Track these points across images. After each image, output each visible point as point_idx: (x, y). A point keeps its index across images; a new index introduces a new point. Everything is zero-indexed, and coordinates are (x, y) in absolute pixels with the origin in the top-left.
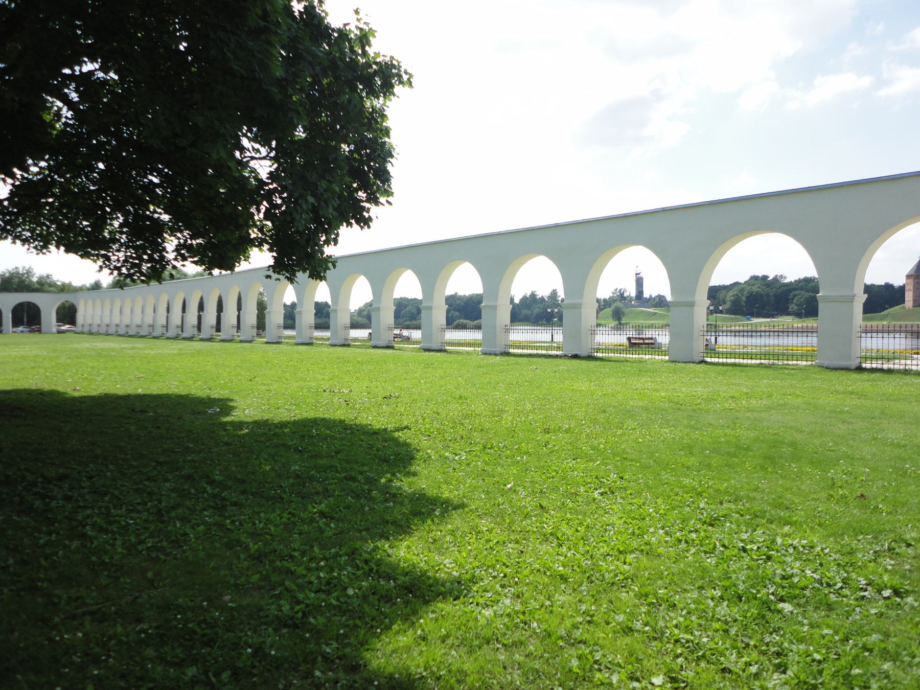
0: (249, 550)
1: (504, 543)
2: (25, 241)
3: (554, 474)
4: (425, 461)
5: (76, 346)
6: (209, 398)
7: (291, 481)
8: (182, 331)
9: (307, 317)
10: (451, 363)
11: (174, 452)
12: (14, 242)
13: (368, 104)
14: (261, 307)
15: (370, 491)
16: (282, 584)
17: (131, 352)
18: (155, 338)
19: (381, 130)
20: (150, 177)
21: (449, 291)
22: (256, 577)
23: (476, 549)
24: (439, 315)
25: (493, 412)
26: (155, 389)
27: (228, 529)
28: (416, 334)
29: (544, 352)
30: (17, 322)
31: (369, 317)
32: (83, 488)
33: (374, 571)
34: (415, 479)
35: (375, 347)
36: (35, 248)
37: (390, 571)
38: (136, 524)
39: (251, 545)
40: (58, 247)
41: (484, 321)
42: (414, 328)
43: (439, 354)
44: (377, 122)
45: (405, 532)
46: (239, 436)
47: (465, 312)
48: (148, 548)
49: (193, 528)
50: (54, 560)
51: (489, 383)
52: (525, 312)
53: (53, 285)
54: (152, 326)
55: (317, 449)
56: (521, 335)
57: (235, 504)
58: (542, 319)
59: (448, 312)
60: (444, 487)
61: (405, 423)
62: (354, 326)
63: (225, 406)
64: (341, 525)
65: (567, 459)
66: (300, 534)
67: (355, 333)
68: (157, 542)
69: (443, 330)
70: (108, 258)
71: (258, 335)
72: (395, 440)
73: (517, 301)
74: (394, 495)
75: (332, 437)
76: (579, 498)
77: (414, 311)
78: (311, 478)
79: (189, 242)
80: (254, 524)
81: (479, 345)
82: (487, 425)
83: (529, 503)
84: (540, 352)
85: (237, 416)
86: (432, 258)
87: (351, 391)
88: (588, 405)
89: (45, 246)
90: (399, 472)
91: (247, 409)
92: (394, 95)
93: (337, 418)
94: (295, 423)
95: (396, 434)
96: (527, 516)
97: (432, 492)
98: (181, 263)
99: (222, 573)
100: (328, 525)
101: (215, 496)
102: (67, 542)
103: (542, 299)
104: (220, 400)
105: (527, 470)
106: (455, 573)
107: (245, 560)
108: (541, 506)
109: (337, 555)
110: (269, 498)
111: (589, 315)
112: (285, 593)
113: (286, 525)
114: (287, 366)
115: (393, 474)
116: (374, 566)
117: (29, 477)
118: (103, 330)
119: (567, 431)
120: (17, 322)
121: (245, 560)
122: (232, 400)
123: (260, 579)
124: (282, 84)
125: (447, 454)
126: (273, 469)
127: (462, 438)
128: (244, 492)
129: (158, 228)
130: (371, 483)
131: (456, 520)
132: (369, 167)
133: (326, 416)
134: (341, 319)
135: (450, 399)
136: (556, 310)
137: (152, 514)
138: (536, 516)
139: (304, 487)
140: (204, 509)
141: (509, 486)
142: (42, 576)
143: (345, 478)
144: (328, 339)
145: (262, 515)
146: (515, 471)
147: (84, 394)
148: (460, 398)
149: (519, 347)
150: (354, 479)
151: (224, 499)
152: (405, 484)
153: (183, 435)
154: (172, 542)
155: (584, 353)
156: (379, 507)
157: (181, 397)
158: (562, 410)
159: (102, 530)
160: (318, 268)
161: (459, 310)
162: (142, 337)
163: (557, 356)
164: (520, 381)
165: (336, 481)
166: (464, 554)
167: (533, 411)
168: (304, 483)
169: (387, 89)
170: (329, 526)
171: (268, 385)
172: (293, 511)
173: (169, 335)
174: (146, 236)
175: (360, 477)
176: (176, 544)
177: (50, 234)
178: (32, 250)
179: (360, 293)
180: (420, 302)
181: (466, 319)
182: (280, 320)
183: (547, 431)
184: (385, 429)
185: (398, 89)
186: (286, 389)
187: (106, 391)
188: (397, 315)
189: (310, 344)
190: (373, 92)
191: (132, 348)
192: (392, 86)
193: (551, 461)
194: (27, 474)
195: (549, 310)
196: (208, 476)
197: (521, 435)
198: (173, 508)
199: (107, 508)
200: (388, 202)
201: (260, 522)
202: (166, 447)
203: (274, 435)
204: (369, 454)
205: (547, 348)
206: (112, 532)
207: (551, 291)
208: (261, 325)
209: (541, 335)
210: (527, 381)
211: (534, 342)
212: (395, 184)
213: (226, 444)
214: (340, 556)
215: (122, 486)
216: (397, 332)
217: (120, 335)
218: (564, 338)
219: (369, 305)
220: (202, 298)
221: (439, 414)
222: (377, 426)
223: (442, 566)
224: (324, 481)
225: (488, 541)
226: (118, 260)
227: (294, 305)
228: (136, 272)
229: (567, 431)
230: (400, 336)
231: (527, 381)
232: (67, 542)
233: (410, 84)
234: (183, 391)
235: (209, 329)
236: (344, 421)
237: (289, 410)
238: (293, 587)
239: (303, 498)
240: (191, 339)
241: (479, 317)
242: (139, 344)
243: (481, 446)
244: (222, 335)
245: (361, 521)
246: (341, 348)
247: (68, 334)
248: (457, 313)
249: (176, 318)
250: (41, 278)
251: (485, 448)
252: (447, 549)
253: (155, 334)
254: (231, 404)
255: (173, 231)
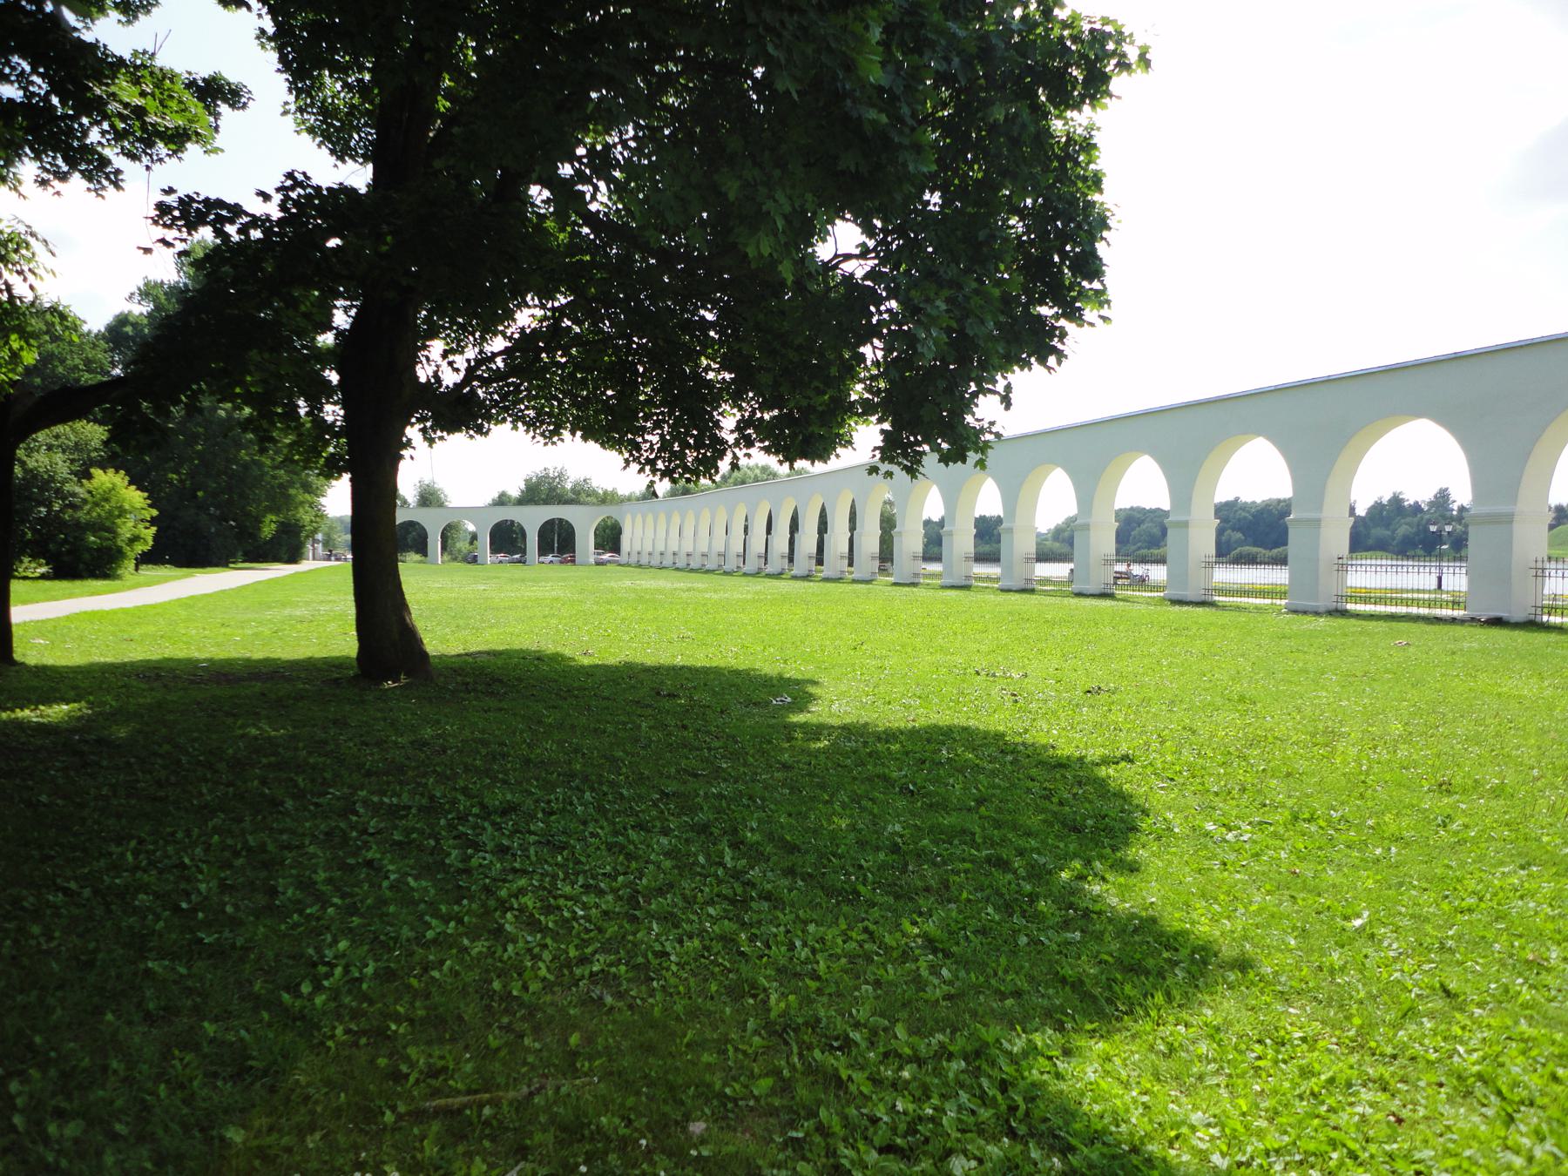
0: (769, 1010)
1: (1349, 1085)
2: (530, 425)
3: (1471, 901)
4: (1159, 838)
5: (613, 584)
6: (780, 678)
7: (882, 856)
8: (851, 564)
9: (962, 541)
10: (1223, 627)
11: (696, 776)
12: (515, 428)
13: (1057, 126)
14: (888, 524)
15: (1033, 898)
16: (813, 1114)
17: (684, 595)
18: (726, 573)
19: (1085, 179)
20: (702, 312)
21: (1223, 495)
22: (765, 1084)
23: (1275, 1092)
24: (1203, 537)
25: (1313, 735)
26: (700, 658)
27: (742, 954)
28: (1158, 573)
29: (1424, 611)
30: (545, 548)
31: (1070, 542)
32: (531, 833)
33: (1020, 1113)
34: (1132, 880)
35: (1079, 595)
36: (542, 435)
37: (1057, 1121)
38: (587, 918)
39: (773, 998)
40: (573, 433)
41: (1293, 548)
42: (1152, 562)
43: (1200, 610)
44: (1077, 163)
45: (1101, 1015)
46: (810, 753)
47: (1256, 533)
48: (592, 974)
49: (681, 942)
50: (432, 978)
51: (1304, 670)
52: (1379, 532)
53: (592, 493)
54: (723, 555)
55: (942, 790)
56: (1371, 575)
57: (767, 897)
58: (1415, 546)
59: (1220, 532)
60: (1200, 904)
61: (1124, 749)
62: (1044, 556)
63: (799, 693)
64: (962, 974)
65: (1502, 863)
66: (877, 984)
67: (1044, 570)
68: (611, 965)
69: (1209, 565)
70: (638, 448)
71: (882, 570)
72: (1101, 784)
73: (1361, 511)
74: (1086, 913)
75: (977, 769)
76: (1548, 979)
77: (1156, 531)
78: (920, 855)
79: (759, 415)
80: (792, 947)
81: (1282, 594)
82: (1302, 765)
83: (1414, 977)
84: (1414, 610)
85: (816, 714)
86: (1189, 431)
87: (1026, 676)
88: (1543, 731)
89: (556, 432)
90: (1102, 857)
91: (837, 704)
92: (1111, 96)
93: (992, 728)
94: (913, 734)
95: (1103, 772)
96: (1409, 1013)
97: (1173, 920)
98: (745, 451)
99: (706, 1058)
100: (934, 970)
101: (736, 874)
102: (466, 942)
103: (1417, 508)
104: (798, 682)
105: (1401, 884)
106: (1216, 1159)
107: (756, 1032)
108: (1447, 993)
109: (944, 1054)
110: (829, 892)
111: (1532, 538)
112: (817, 1139)
113: (852, 958)
114: (922, 625)
115: (1088, 863)
116: (1019, 1099)
117: (463, 803)
118: (656, 561)
119: (1497, 792)
120: (545, 548)
121: (756, 1032)
122: (815, 683)
123: (773, 1092)
124: (885, 98)
125: (1210, 827)
126: (853, 828)
127: (1243, 790)
128: (790, 872)
129: (714, 396)
130: (1039, 877)
131: (1222, 1007)
132: (1064, 256)
133: (971, 723)
134: (1020, 544)
135: (1219, 701)
136: (1448, 528)
137: (620, 898)
138: (1432, 1015)
139: (904, 870)
140: (711, 903)
141: (1357, 923)
142: (401, 1010)
143: (988, 860)
144: (998, 580)
145: (811, 928)
146: (1370, 883)
147: (597, 662)
148: (1242, 699)
149: (1366, 600)
150: (1003, 865)
151: (750, 884)
152: (1111, 893)
153: (716, 744)
154: (636, 967)
155: (1518, 615)
156: (1051, 940)
157: (737, 673)
158: (1477, 740)
159: (533, 925)
160: (963, 444)
161: (1239, 530)
162: (708, 572)
163: (1453, 620)
164: (1373, 669)
165: (968, 865)
166: (1243, 1104)
167: (1407, 738)
168: (906, 865)
169: (1096, 86)
170: (939, 975)
171: (880, 658)
172: (872, 927)
173: (746, 569)
174: (691, 411)
175: (1017, 863)
176: (643, 974)
177: (563, 412)
178: (539, 438)
179: (1054, 501)
180: (1166, 514)
181: (1255, 545)
182: (918, 547)
183: (1445, 788)
184: (1081, 759)
185: (1118, 83)
186: (910, 666)
187: (630, 659)
188: (1122, 538)
189: (966, 587)
190: (1065, 99)
191: (689, 590)
192: (1106, 79)
193: (1463, 864)
194: (461, 798)
195: (1433, 528)
196: (735, 831)
197: (1382, 794)
198: (661, 892)
199: (554, 877)
200: (1104, 319)
201: (805, 944)
202: (683, 763)
203: (870, 755)
204: (1043, 811)
205: (1430, 604)
206: (544, 930)
207: (1435, 491)
208: (886, 555)
209: (1415, 578)
210: (1387, 671)
211: (1402, 591)
212: (1113, 279)
213: (786, 767)
214: (950, 1057)
215: (593, 835)
216: (1122, 568)
217: (677, 569)
218: (1470, 582)
219: (1070, 521)
220: (823, 510)
221: (1194, 732)
222: (1065, 750)
223: (1184, 1130)
224: (945, 863)
225: (1307, 1073)
226: (651, 449)
227: (941, 523)
228: (677, 466)
229: (1497, 792)
230: (1127, 575)
231: (1387, 671)
232: (466, 942)
233: (1144, 60)
234: (742, 664)
235: (804, 559)
236: (1003, 735)
237: (907, 707)
238: (837, 1127)
239: (897, 897)
240: (778, 576)
241: (1282, 540)
242: (700, 582)
243: (1287, 813)
244: (826, 571)
245: (1006, 971)
246: (1017, 596)
247: (609, 567)
248: (1239, 535)
249: (757, 544)
250: (576, 484)
251: (1296, 818)
252: (1200, 1078)
253: (727, 568)
254: (811, 689)
255: (737, 399)
